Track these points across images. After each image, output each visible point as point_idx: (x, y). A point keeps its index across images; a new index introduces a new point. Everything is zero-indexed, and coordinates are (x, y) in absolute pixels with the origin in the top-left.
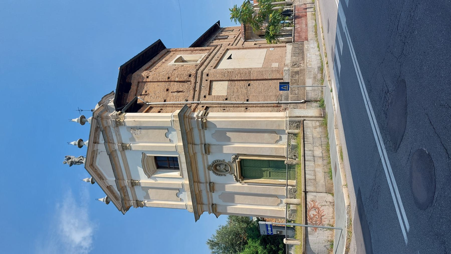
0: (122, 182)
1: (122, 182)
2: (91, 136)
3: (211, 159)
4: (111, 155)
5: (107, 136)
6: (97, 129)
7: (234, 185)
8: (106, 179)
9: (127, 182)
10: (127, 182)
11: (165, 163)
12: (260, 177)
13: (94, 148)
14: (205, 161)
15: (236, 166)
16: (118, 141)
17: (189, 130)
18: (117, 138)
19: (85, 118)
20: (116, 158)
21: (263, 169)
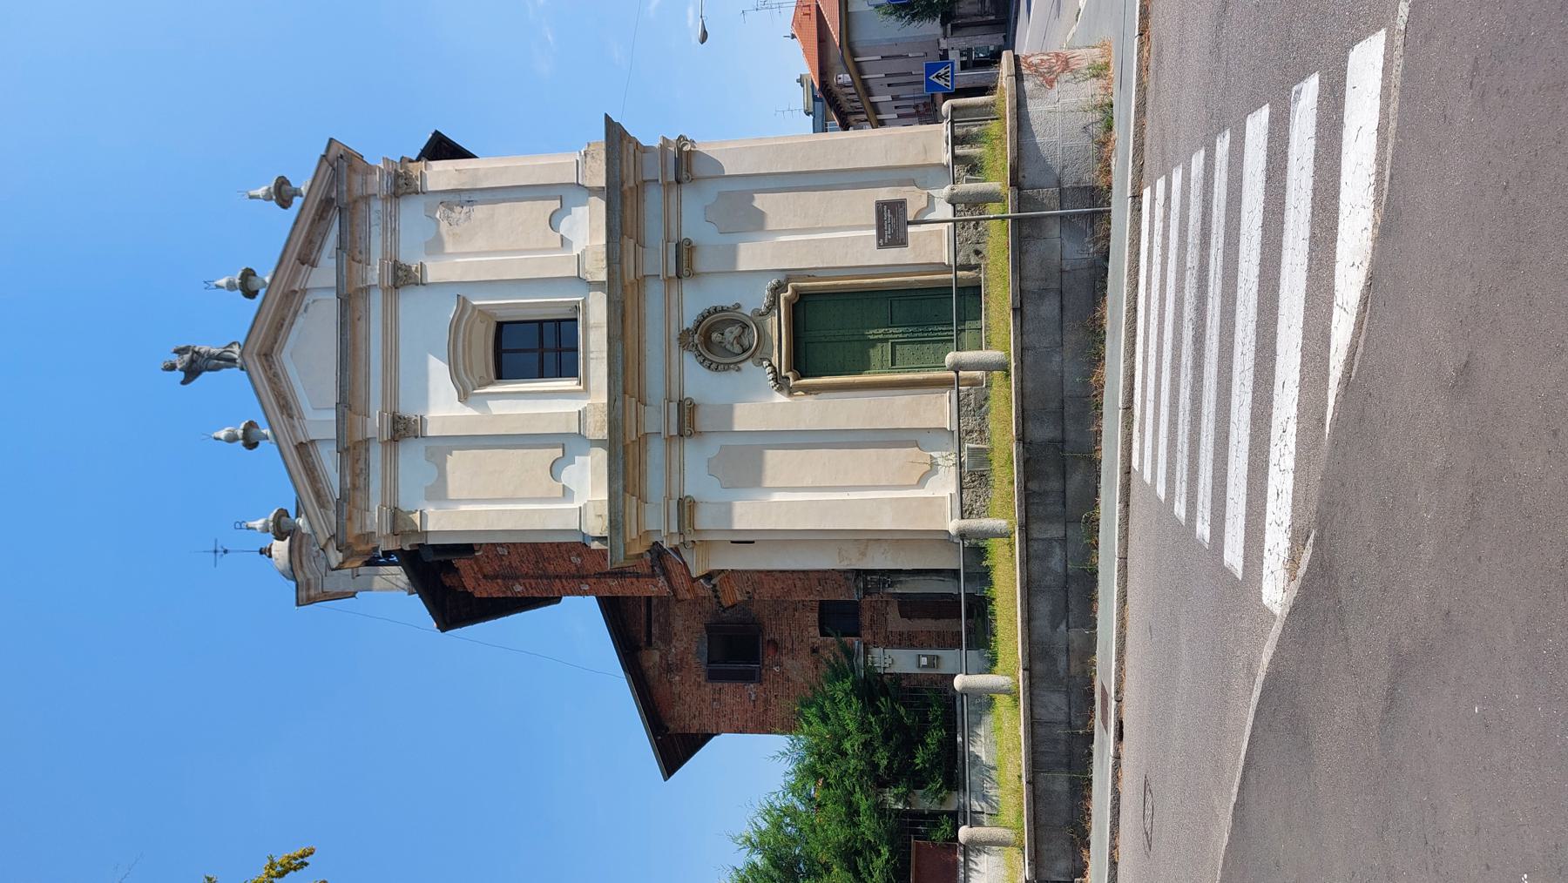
0: (359, 419)
1: (359, 419)
2: (300, 226)
3: (694, 302)
4: (350, 302)
5: (352, 233)
6: (326, 205)
7: (760, 404)
8: (301, 417)
9: (375, 423)
10: (375, 423)
11: (529, 346)
12: (859, 372)
13: (293, 281)
14: (674, 312)
15: (776, 328)
16: (384, 252)
17: (632, 184)
18: (385, 241)
19: (288, 183)
20: (362, 324)
21: (873, 334)
